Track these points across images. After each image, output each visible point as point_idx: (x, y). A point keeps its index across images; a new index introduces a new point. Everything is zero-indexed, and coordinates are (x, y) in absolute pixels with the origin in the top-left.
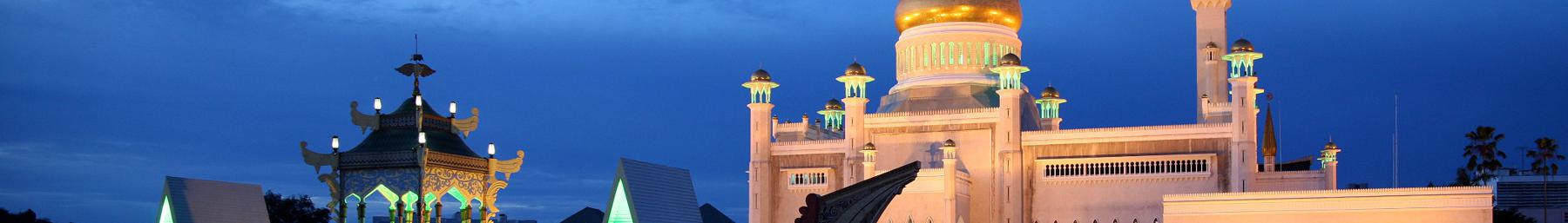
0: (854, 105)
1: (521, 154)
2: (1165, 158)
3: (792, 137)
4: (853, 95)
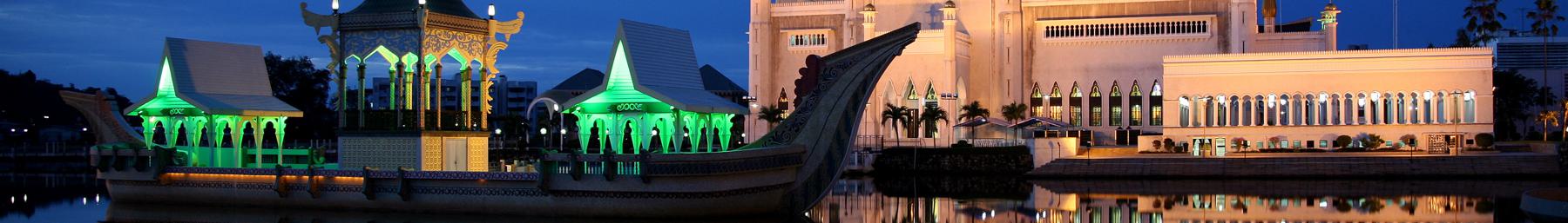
1: (521, 15)
2: (1165, 19)
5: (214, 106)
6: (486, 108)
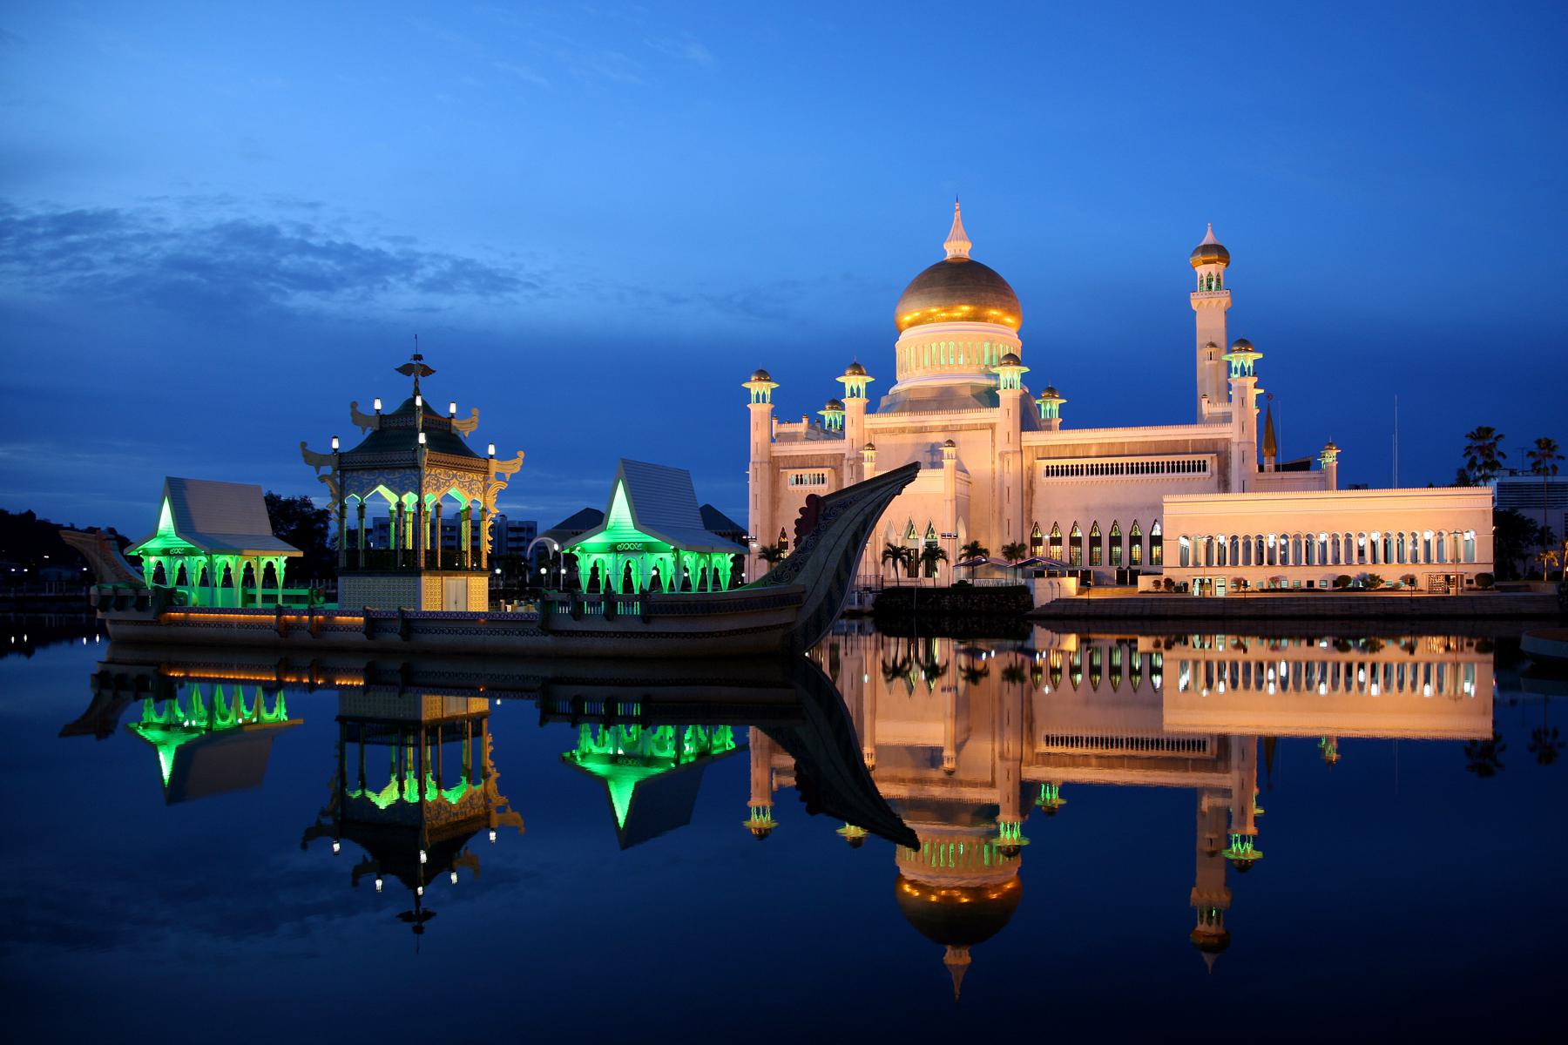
0: (854, 405)
1: (521, 454)
3: (792, 438)
4: (853, 395)
5: (214, 546)
6: (486, 548)
